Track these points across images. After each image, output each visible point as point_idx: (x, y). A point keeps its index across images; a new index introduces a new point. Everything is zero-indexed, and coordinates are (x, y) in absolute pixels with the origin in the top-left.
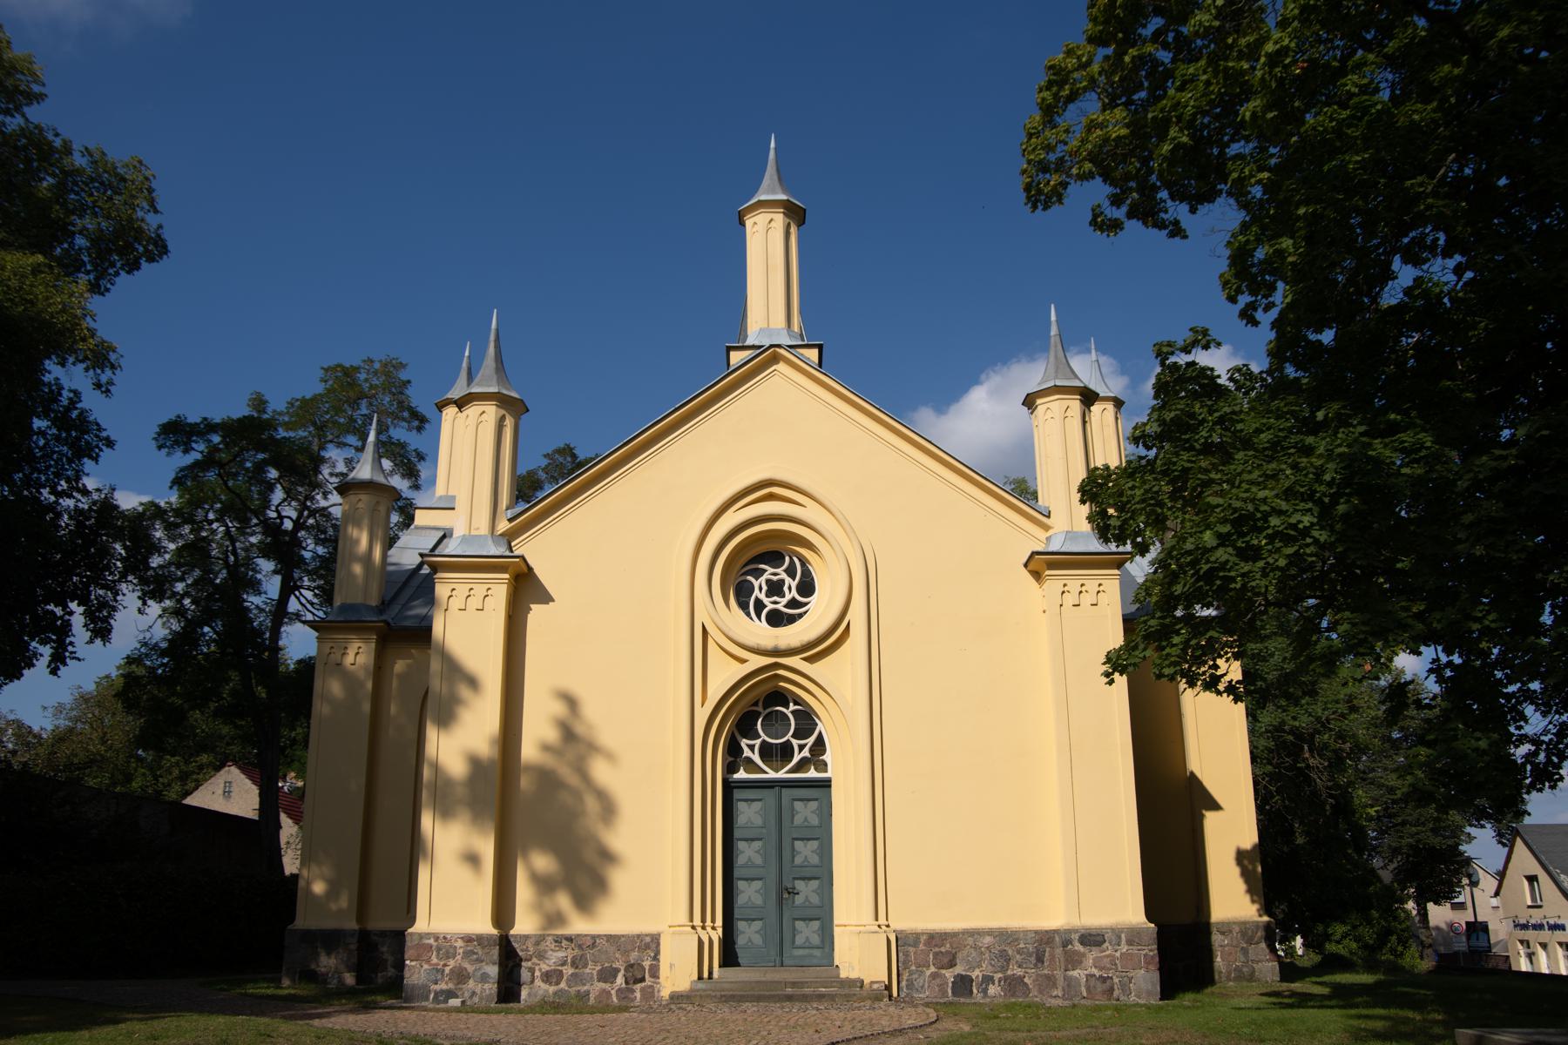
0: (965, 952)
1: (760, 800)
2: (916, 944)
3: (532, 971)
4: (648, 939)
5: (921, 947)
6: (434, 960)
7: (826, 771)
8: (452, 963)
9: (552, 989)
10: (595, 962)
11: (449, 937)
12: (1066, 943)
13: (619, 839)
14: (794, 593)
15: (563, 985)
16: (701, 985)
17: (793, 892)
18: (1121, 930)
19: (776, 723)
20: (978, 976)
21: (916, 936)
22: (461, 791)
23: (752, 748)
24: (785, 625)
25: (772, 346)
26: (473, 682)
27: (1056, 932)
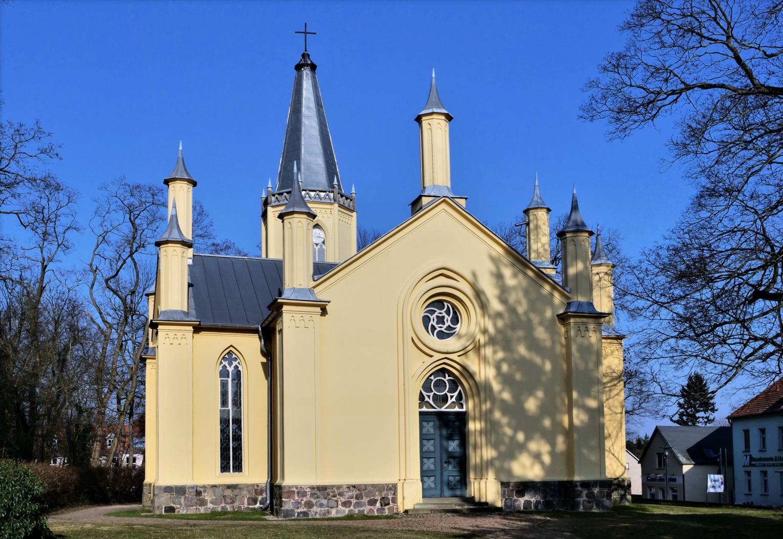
4: (391, 486)
8: (305, 499)
9: (347, 510)
10: (367, 497)
11: (303, 487)
14: (439, 329)
15: (352, 508)
20: (534, 501)
24: (445, 339)
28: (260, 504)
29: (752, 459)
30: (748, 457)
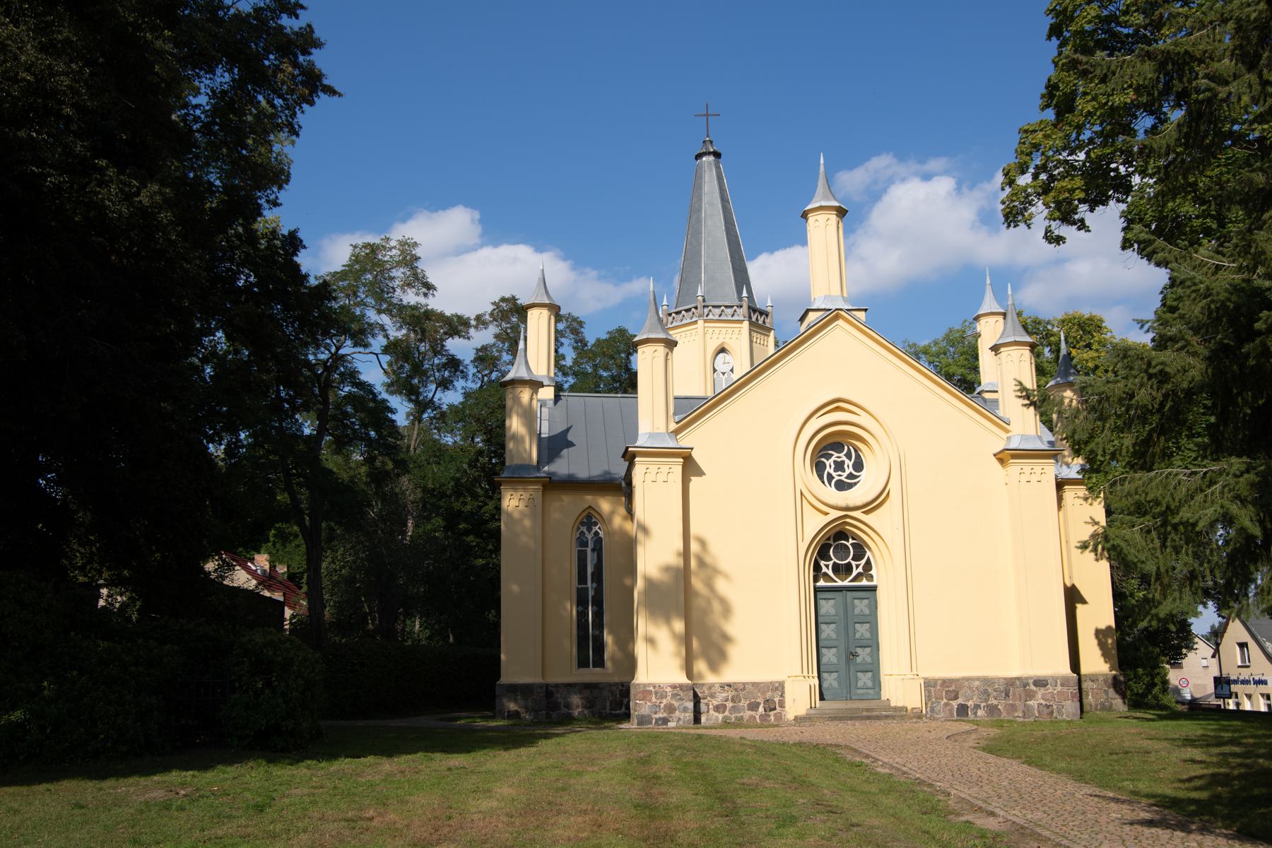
0: (963, 691)
1: (834, 599)
2: (935, 686)
3: (707, 705)
4: (777, 685)
5: (938, 687)
6: (654, 700)
7: (872, 581)
8: (665, 701)
12: (1025, 685)
13: (733, 628)
14: (851, 470)
15: (727, 713)
16: (812, 711)
17: (855, 655)
18: (1058, 678)
21: (935, 681)
23: (827, 566)
25: (837, 309)
27: (1018, 679)
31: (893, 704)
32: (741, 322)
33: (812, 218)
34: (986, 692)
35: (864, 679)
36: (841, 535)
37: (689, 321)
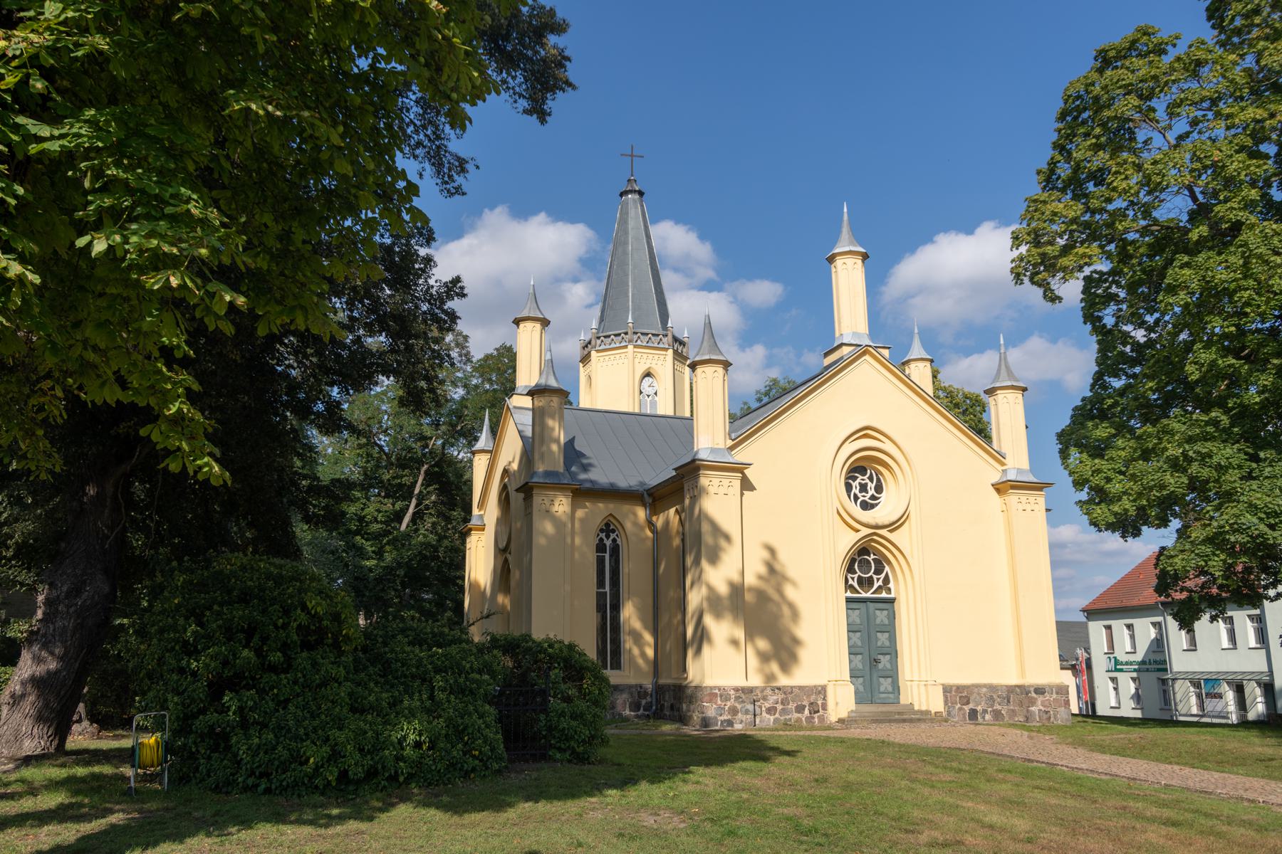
2: (950, 692)
3: (761, 707)
8: (729, 704)
13: (801, 632)
14: (862, 498)
15: (777, 715)
19: (865, 565)
21: (951, 687)
22: (726, 603)
26: (728, 538)
27: (1018, 686)
28: (644, 710)
29: (1117, 662)
30: (1113, 660)
31: (916, 708)
32: (666, 349)
33: (839, 262)
34: (991, 698)
35: (886, 684)
36: (864, 551)
37: (618, 345)
